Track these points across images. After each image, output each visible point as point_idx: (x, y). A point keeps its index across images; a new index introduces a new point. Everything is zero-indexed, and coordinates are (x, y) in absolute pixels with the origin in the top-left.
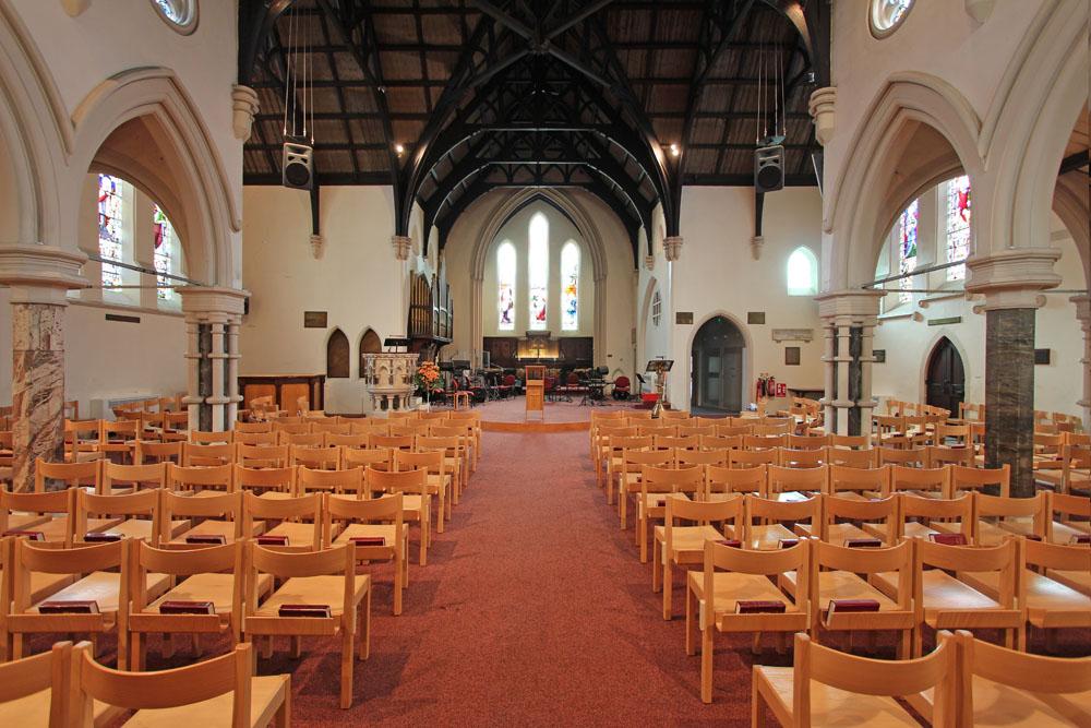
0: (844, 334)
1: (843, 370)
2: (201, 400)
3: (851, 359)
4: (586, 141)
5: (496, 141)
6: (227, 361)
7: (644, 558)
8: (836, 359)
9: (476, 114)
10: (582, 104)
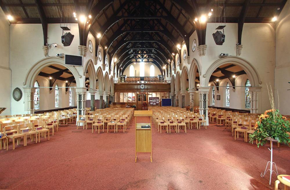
0: (202, 95)
2: (79, 109)
4: (156, 35)
5: (130, 35)
9: (124, 28)
10: (153, 35)
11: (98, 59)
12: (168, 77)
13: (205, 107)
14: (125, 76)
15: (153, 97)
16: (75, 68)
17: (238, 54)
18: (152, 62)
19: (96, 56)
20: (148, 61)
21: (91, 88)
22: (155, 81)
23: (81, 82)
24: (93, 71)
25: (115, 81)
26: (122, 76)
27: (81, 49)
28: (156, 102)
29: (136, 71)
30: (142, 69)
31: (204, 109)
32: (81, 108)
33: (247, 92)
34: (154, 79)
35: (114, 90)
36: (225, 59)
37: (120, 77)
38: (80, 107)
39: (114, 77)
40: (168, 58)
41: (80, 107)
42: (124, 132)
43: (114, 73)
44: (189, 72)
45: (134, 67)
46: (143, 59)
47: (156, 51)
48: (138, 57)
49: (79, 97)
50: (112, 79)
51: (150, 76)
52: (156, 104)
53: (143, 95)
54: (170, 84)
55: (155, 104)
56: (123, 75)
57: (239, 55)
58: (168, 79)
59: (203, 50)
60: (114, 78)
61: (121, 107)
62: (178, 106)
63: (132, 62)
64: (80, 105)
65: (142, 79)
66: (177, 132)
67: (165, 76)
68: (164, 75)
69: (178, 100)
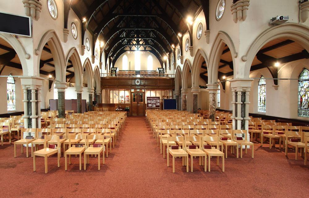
0: (239, 94)
1: (239, 107)
2: (28, 117)
3: (242, 103)
6: (37, 103)
7: (161, 153)
8: (237, 103)
11: (85, 48)
12: (170, 69)
13: (243, 115)
14: (117, 68)
15: (151, 96)
16: (19, 41)
17: (301, 20)
18: (150, 51)
19: (66, 26)
20: (145, 50)
21: (57, 80)
22: (154, 75)
23: (30, 66)
24: (91, 71)
25: (102, 74)
26: (112, 69)
27: (28, 5)
28: (155, 104)
29: (130, 62)
30: (138, 60)
31: (242, 119)
32: (31, 114)
33: (303, 89)
34: (153, 72)
35: (101, 87)
36: (278, 28)
37: (110, 69)
38: (29, 113)
39: (101, 68)
40: (171, 42)
41: (29, 113)
42: (99, 169)
43: (100, 63)
44: (208, 59)
45: (127, 56)
46: (139, 46)
47: (153, 41)
48: (132, 44)
49: (28, 94)
50: (97, 70)
51: (148, 70)
52: (157, 106)
53: (139, 94)
54: (173, 79)
55: (154, 106)
56: (115, 67)
57: (304, 21)
58: (170, 73)
59: (242, 11)
60: (100, 70)
61: (109, 111)
62: (186, 110)
63: (125, 51)
64: (29, 109)
65: (138, 72)
66: (206, 170)
67: (166, 69)
68: (165, 69)
69: (185, 102)
